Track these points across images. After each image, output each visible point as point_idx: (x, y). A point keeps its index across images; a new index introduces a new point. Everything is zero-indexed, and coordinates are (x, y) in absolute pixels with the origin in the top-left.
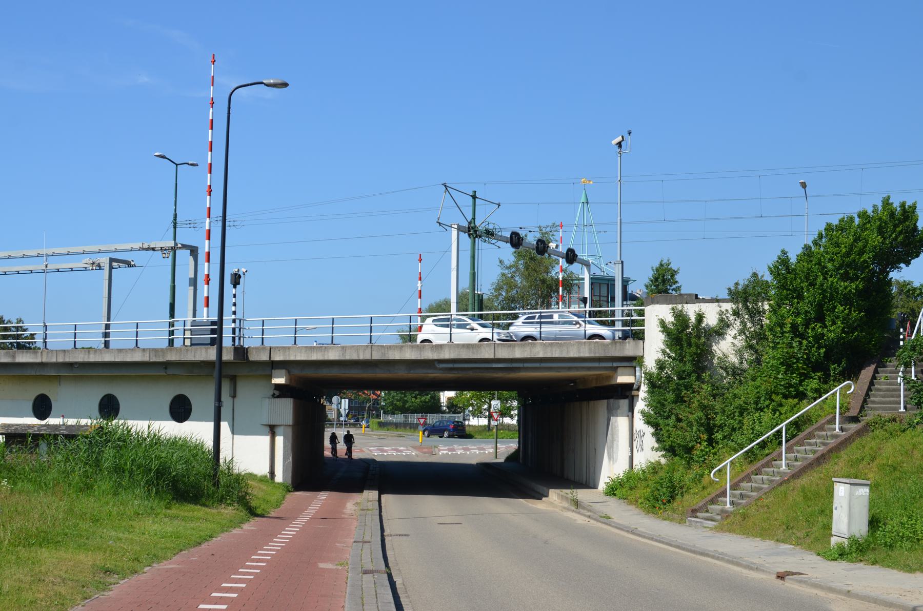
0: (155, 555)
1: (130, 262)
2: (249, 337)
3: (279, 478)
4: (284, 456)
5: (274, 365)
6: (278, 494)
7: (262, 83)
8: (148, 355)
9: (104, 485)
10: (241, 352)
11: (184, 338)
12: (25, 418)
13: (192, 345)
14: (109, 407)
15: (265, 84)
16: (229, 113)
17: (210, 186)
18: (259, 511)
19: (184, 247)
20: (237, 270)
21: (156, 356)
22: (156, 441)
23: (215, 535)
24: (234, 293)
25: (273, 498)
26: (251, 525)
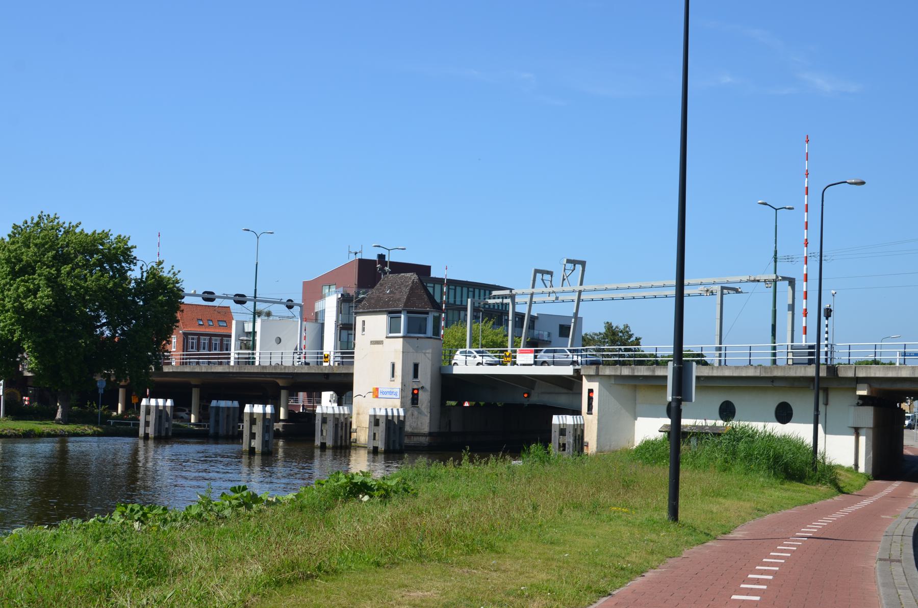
0: (781, 506)
1: (737, 289)
2: (838, 358)
3: (862, 469)
4: (866, 452)
5: (858, 381)
6: (861, 481)
7: (846, 182)
8: (759, 371)
9: (738, 467)
10: (833, 370)
11: (788, 359)
12: (660, 419)
13: (793, 364)
14: (727, 411)
15: (848, 183)
16: (822, 205)
17: (807, 240)
18: (845, 490)
19: (784, 279)
20: (828, 306)
21: (765, 372)
22: (770, 438)
23: (815, 501)
24: (826, 323)
25: (856, 484)
26: (839, 498)
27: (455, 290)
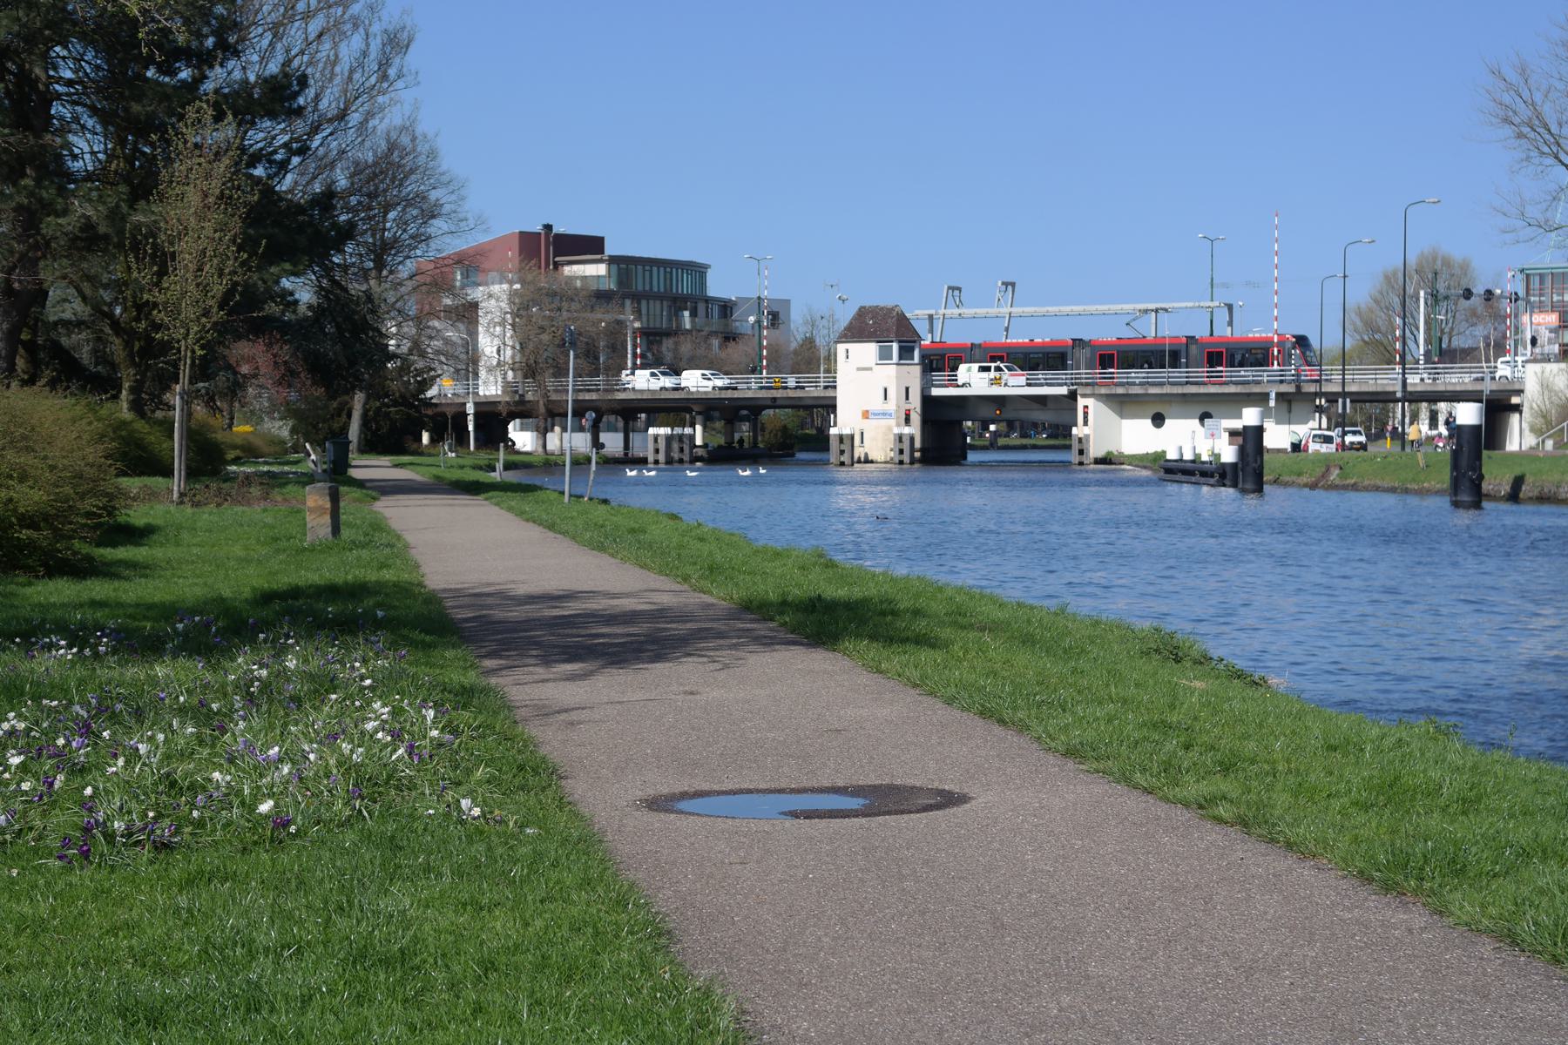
27: (651, 271)
